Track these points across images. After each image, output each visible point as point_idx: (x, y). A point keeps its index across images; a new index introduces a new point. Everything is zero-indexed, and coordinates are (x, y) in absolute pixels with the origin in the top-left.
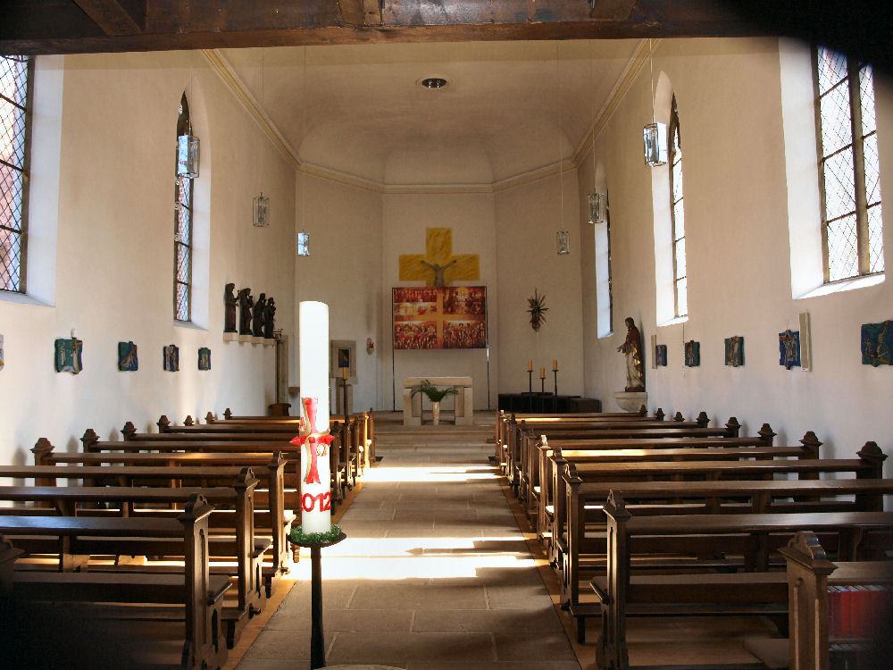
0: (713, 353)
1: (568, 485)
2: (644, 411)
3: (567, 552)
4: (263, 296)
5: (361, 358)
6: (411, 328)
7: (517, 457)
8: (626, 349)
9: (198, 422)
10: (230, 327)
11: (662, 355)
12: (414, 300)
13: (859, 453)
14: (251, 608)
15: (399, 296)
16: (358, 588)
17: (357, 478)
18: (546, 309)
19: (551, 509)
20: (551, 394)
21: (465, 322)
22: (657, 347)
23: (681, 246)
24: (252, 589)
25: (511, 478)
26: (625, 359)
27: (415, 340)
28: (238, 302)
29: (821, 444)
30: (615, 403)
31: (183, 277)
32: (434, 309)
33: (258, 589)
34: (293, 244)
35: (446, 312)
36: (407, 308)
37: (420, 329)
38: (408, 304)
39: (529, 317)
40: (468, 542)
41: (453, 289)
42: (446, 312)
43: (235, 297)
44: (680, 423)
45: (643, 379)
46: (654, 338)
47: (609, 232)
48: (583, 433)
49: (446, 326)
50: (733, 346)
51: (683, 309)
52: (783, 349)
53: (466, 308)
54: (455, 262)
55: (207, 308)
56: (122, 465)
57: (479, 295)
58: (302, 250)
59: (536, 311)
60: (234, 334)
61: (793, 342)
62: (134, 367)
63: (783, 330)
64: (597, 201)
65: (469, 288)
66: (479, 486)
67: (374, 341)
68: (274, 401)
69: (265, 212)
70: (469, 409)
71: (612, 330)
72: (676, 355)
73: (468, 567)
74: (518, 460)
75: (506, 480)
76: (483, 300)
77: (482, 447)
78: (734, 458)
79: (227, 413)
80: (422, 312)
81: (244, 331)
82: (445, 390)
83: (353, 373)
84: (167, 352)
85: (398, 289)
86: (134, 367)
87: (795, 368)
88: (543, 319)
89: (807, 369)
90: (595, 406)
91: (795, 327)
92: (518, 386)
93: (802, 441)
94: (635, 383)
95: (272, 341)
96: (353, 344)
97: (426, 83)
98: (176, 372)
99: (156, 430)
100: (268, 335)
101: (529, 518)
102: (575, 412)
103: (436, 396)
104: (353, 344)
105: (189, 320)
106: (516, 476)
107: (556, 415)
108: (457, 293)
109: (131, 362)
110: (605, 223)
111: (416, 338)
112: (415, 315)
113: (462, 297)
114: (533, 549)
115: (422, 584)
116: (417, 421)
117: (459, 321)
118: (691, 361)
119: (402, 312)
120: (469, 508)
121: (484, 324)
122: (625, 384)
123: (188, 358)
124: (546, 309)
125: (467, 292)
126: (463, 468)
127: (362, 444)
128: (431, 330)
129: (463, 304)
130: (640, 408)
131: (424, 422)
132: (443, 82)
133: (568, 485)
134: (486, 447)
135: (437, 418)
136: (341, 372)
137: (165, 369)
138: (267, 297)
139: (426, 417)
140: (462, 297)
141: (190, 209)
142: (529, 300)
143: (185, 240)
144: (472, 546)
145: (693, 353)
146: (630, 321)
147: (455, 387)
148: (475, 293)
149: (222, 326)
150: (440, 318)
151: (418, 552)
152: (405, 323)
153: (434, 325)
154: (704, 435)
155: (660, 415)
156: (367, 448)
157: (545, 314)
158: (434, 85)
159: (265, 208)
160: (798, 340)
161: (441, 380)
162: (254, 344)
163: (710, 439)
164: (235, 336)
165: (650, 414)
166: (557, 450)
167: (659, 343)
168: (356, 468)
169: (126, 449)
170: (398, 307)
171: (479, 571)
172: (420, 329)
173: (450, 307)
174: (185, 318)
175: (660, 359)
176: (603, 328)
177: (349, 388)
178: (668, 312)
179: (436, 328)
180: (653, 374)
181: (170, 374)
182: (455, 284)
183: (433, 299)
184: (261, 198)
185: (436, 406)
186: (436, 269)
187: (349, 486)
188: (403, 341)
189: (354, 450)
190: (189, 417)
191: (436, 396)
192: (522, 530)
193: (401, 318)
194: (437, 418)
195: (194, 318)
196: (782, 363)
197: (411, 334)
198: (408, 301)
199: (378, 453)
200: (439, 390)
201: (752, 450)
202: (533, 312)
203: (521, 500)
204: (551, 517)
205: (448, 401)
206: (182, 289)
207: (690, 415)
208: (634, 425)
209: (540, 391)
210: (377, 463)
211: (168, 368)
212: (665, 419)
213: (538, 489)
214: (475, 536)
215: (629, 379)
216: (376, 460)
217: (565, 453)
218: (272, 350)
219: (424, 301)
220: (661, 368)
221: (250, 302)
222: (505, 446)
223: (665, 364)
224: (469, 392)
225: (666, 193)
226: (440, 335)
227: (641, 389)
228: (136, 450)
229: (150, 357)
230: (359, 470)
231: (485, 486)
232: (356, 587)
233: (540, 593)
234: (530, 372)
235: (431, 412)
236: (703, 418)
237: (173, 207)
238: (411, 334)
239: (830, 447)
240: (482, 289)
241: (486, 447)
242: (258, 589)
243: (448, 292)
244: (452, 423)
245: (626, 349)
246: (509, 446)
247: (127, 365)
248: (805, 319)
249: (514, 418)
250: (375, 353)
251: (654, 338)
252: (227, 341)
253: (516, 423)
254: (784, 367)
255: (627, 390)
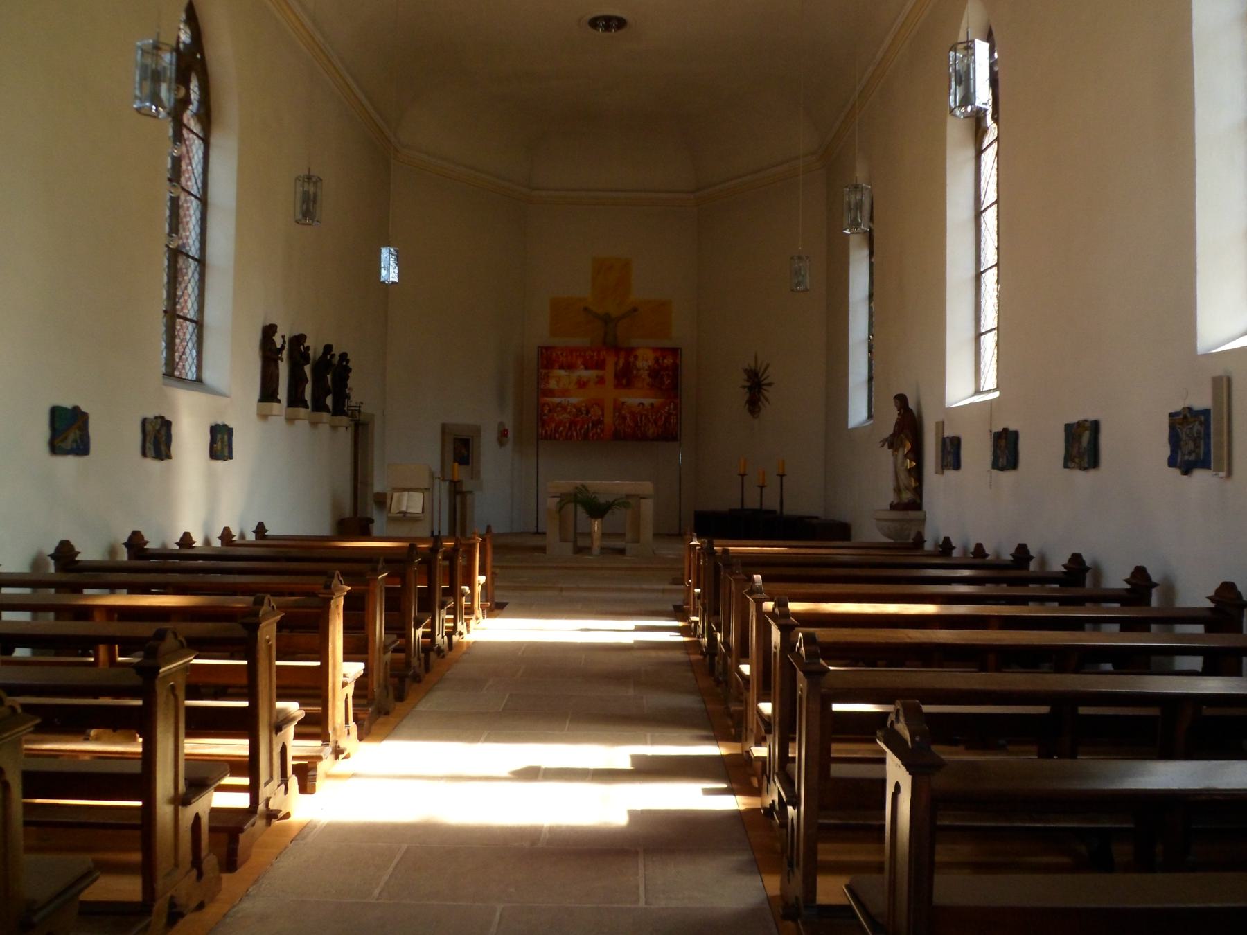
0: (1042, 448)
1: (800, 674)
2: (919, 541)
3: (796, 805)
4: (328, 348)
5: (490, 454)
6: (564, 409)
7: (713, 609)
8: (893, 442)
9: (242, 536)
10: (268, 394)
11: (951, 453)
12: (571, 367)
13: (1211, 599)
14: (172, 904)
15: (547, 359)
16: (407, 851)
17: (456, 638)
18: (770, 384)
19: (766, 708)
20: (774, 512)
21: (648, 401)
22: (944, 440)
23: (990, 278)
24: (176, 865)
25: (705, 641)
26: (891, 459)
27: (570, 428)
28: (285, 354)
29: (1155, 585)
30: (871, 525)
31: (189, 307)
32: (601, 381)
33: (197, 862)
34: (375, 265)
35: (618, 385)
36: (560, 378)
37: (579, 410)
38: (562, 372)
39: (744, 395)
40: (620, 755)
41: (630, 351)
42: (618, 385)
43: (279, 346)
44: (978, 561)
45: (918, 490)
46: (941, 426)
47: (871, 264)
48: (825, 572)
49: (618, 407)
50: (1080, 436)
51: (990, 379)
52: (1175, 440)
53: (649, 380)
54: (635, 310)
55: (230, 363)
56: (51, 615)
57: (668, 361)
58: (390, 273)
59: (756, 386)
60: (275, 405)
61: (1197, 427)
62: (82, 448)
63: (1178, 407)
64: (858, 197)
65: (655, 349)
66: (653, 654)
67: (509, 425)
68: (347, 512)
69: (315, 201)
70: (647, 533)
71: (870, 416)
72: (977, 452)
73: (609, 808)
74: (717, 613)
75: (697, 644)
76: (675, 370)
77: (664, 591)
78: (1022, 601)
79: (260, 530)
80: (582, 384)
81: (295, 400)
82: (611, 501)
83: (475, 475)
84: (149, 427)
85: (547, 348)
86: (82, 448)
87: (1199, 475)
88: (767, 400)
89: (1222, 474)
90: (841, 531)
91: (1202, 401)
92: (725, 499)
93: (1127, 581)
94: (907, 496)
95: (345, 420)
96: (477, 431)
97: (594, 23)
98: (165, 462)
99: (123, 556)
100: (338, 410)
101: (730, 715)
102: (818, 546)
103: (597, 510)
104: (477, 431)
105: (199, 380)
106: (712, 639)
107: (781, 543)
108: (636, 357)
109: (75, 441)
110: (866, 252)
111: (573, 423)
112: (571, 388)
113: (645, 360)
114: (736, 773)
115: (526, 844)
116: (568, 547)
117: (638, 399)
118: (1002, 461)
119: (553, 384)
120: (631, 692)
121: (675, 408)
122: (891, 497)
123: (190, 438)
124: (770, 384)
125: (651, 356)
126: (631, 623)
127: (470, 582)
128: (595, 412)
129: (644, 374)
130: (913, 535)
131: (579, 550)
132: (621, 23)
133: (800, 674)
134: (670, 591)
135: (597, 544)
136: (459, 472)
137: (144, 454)
138: (337, 351)
139: (581, 543)
140: (645, 360)
141: (204, 201)
142: (745, 371)
143: (193, 250)
144: (627, 765)
145: (1006, 449)
146: (901, 400)
147: (628, 496)
148: (664, 358)
149: (256, 393)
150: (610, 394)
151: (531, 774)
152: (556, 400)
153: (599, 403)
154: (1024, 582)
155: (946, 547)
156: (478, 589)
157: (769, 393)
158: (607, 28)
159: (315, 195)
160: (1207, 424)
161: (607, 486)
162: (314, 424)
163: (1033, 589)
164: (280, 408)
165: (929, 546)
166: (781, 604)
167: (948, 433)
168: (455, 621)
169: (60, 587)
170: (547, 376)
171: (634, 815)
172: (579, 410)
173: (625, 378)
174: (191, 374)
175: (950, 458)
176: (857, 412)
177: (469, 496)
178: (968, 378)
179: (603, 410)
180: (935, 481)
181: (153, 465)
182: (634, 342)
183: (600, 365)
184: (309, 178)
185: (596, 526)
186: (606, 320)
187: (440, 651)
188: (545, 428)
189: (452, 592)
190: (226, 530)
191: (597, 510)
192: (718, 737)
193: (551, 393)
194: (597, 544)
195: (207, 376)
196: (1172, 462)
197: (565, 417)
198: (561, 367)
199: (499, 597)
200: (602, 500)
201: (1113, 609)
202: (750, 388)
203: (718, 683)
204: (766, 721)
205: (615, 516)
206: (186, 331)
207: (1001, 547)
208: (903, 562)
209: (757, 506)
210: (497, 612)
211: (151, 451)
212: (955, 553)
213: (745, 669)
214: (643, 741)
215: (898, 490)
216: (496, 608)
217: (794, 607)
218: (345, 436)
219: (586, 368)
220: (950, 474)
221: (305, 357)
222: (698, 591)
223: (957, 466)
224: (647, 507)
225: (972, 193)
226: (609, 419)
227: (916, 504)
228: (77, 589)
229: (115, 434)
230: (461, 627)
231: (663, 654)
232: (404, 846)
233: (741, 870)
234: (743, 475)
235: (589, 534)
236: (1022, 554)
237: (165, 193)
238: (565, 417)
239: (1169, 590)
240: (675, 351)
241: (670, 591)
242: (197, 862)
243: (622, 355)
244: (622, 552)
245: (893, 442)
246: (703, 591)
247: (68, 444)
248: (1223, 386)
249: (711, 545)
250: (509, 446)
251: (941, 426)
252: (264, 416)
253: (715, 552)
254: (1176, 472)
255: (893, 507)
